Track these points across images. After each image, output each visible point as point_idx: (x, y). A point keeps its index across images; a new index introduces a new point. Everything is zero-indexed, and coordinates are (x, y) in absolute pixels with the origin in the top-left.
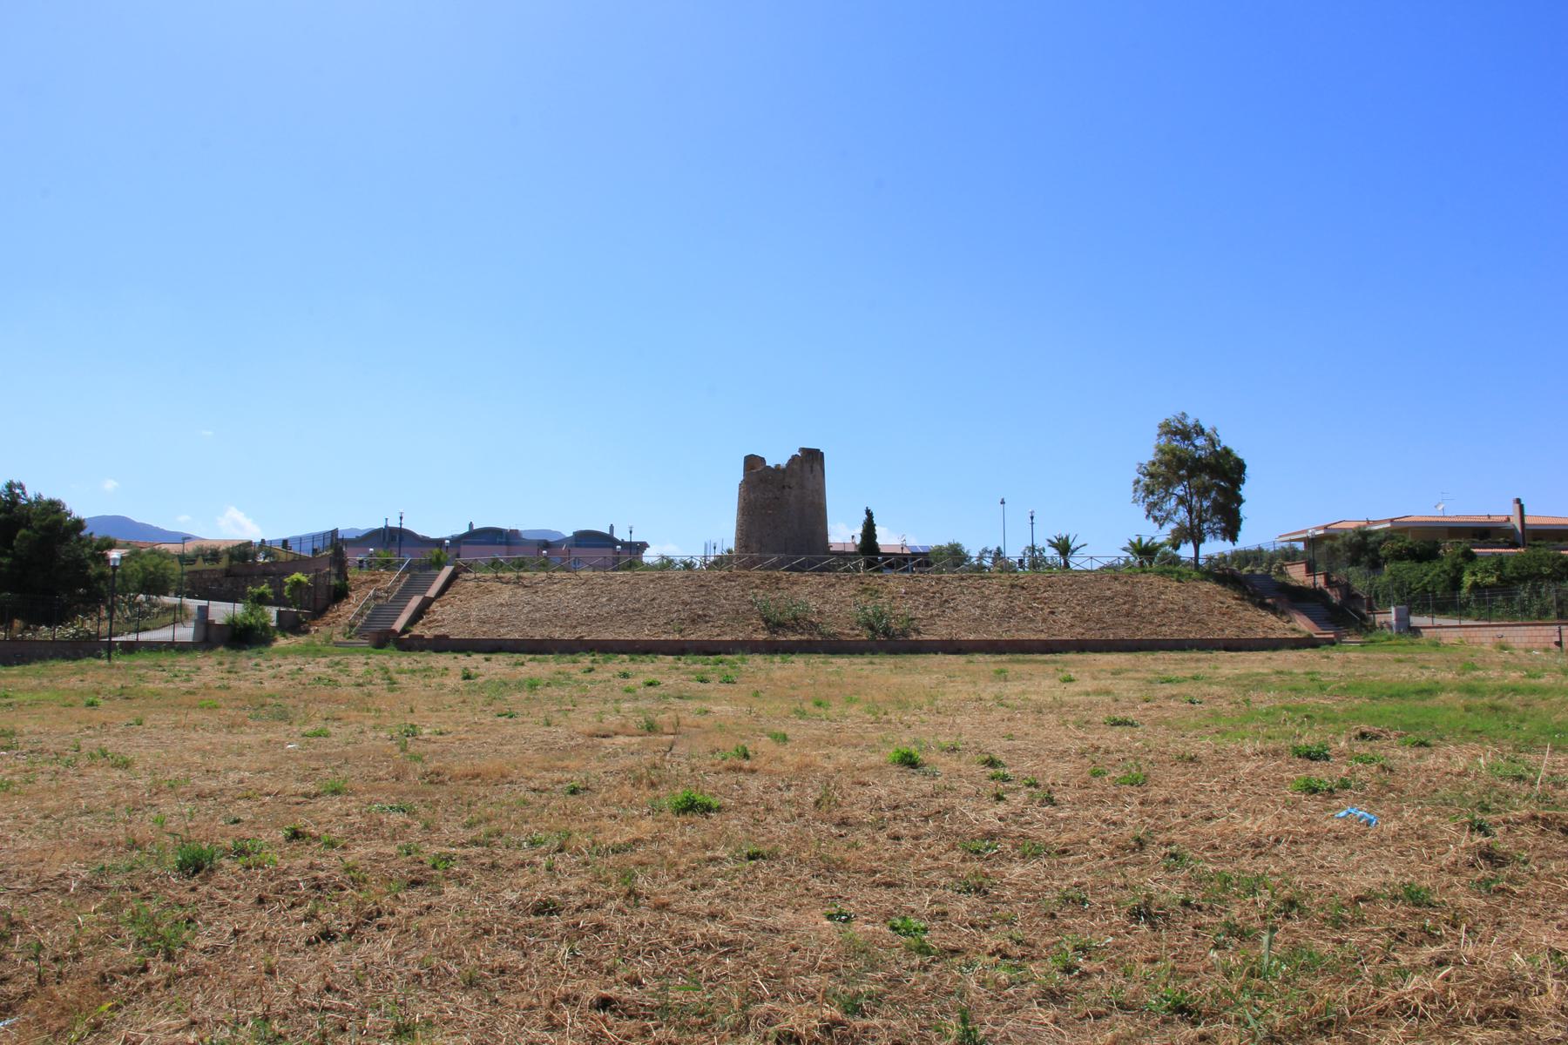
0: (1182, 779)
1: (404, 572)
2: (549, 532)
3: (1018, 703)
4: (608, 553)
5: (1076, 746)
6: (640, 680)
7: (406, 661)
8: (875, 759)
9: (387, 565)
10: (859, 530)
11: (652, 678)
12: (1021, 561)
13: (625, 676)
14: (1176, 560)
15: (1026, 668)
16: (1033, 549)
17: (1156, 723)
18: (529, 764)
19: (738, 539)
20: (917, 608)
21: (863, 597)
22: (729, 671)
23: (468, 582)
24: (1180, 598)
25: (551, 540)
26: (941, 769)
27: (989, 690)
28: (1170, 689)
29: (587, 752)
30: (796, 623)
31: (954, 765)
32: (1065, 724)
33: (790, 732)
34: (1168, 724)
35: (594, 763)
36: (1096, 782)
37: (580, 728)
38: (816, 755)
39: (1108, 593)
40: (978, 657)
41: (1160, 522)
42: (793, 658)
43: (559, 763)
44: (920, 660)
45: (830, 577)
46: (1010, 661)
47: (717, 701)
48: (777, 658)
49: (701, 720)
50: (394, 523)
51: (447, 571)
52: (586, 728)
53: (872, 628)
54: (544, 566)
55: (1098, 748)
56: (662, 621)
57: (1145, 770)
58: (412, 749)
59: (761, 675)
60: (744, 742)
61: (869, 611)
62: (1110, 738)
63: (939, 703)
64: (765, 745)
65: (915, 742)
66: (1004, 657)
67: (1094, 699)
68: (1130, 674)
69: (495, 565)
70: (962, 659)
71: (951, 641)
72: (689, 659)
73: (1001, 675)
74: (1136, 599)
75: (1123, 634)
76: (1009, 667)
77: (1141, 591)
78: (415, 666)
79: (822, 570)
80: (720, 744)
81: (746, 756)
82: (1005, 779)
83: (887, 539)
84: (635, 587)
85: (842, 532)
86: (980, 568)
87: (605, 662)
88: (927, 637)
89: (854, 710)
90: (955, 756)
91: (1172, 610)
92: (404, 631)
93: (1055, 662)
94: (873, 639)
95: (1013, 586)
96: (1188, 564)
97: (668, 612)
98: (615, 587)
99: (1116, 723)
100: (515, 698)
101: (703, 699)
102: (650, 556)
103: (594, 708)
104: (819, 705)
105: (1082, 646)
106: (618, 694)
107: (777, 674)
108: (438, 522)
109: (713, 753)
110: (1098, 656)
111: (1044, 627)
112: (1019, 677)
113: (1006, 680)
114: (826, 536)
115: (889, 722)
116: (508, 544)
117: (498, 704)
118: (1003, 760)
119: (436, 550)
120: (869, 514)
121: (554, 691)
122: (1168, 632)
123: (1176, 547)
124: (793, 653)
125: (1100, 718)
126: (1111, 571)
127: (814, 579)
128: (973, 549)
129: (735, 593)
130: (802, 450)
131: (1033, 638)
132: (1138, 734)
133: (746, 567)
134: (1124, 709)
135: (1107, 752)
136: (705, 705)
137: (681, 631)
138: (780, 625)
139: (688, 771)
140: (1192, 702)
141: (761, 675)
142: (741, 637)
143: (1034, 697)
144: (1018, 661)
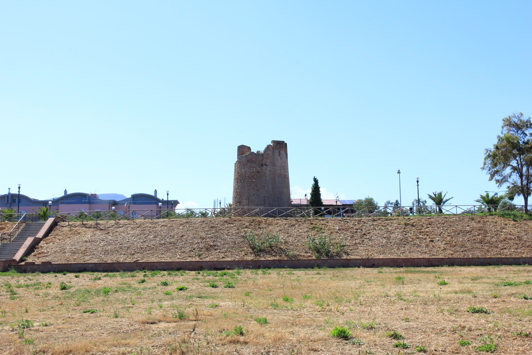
0: (521, 349)
1: (22, 222)
2: (116, 195)
3: (411, 298)
4: (154, 207)
5: (449, 326)
6: (175, 287)
7: (23, 279)
8: (322, 334)
9: (10, 218)
10: (309, 191)
11: (182, 285)
12: (411, 209)
13: (165, 284)
14: (512, 208)
15: (416, 276)
16: (418, 201)
17: (502, 312)
18: (104, 343)
19: (235, 198)
20: (346, 239)
21: (313, 233)
22: (230, 280)
23: (64, 228)
24: (515, 231)
25: (118, 200)
26: (363, 341)
27: (393, 290)
28: (513, 290)
29: (141, 334)
30: (271, 249)
31: (372, 338)
32: (442, 311)
33: (269, 318)
34: (510, 312)
35: (146, 341)
36: (464, 349)
37: (136, 319)
38: (284, 332)
39: (468, 228)
40: (385, 269)
41: (500, 182)
42: (270, 271)
43: (123, 342)
44: (348, 271)
45: (292, 221)
46: (406, 272)
47: (222, 299)
48: (260, 272)
49: (212, 311)
50: (14, 191)
51: (50, 221)
52: (141, 318)
53: (318, 252)
54: (113, 216)
55: (464, 327)
56: (188, 249)
57: (495, 341)
58: (27, 336)
59: (250, 282)
60: (239, 325)
61: (317, 241)
62: (473, 321)
63: (361, 299)
64: (253, 327)
65: (347, 323)
66: (402, 269)
67: (460, 295)
68: (484, 280)
69: (81, 216)
70: (375, 271)
71: (368, 259)
72: (205, 273)
73: (400, 281)
74: (486, 232)
75: (478, 254)
76: (405, 275)
77: (490, 227)
78: (29, 282)
79: (287, 216)
80: (225, 326)
81: (242, 334)
82: (405, 347)
83: (327, 197)
84: (171, 229)
85: (299, 193)
86: (386, 213)
87: (153, 276)
88: (353, 257)
89: (308, 303)
90: (372, 332)
91: (511, 239)
92: (22, 260)
93: (435, 272)
94: (318, 259)
95: (406, 224)
96: (521, 209)
97: (192, 243)
98: (159, 228)
99: (476, 311)
100: (95, 301)
101: (214, 298)
102: (180, 209)
103: (146, 305)
104: (287, 300)
105: (452, 262)
106: (161, 296)
107: (260, 281)
108: (43, 189)
109: (221, 332)
110: (462, 268)
111: (427, 250)
112: (411, 282)
113: (403, 284)
114: (289, 194)
115: (330, 310)
116: (89, 203)
117: (84, 305)
118: (403, 335)
119: (44, 209)
120: (316, 181)
121: (120, 296)
122: (509, 253)
123: (512, 198)
124: (270, 268)
125: (465, 307)
126: (469, 215)
127: (282, 222)
128: (381, 203)
129: (233, 231)
130: (273, 142)
131: (420, 257)
132: (490, 319)
133: (239, 215)
134: (480, 302)
135: (470, 330)
136: (216, 302)
137: (200, 256)
138: (261, 251)
139: (205, 344)
140: (526, 298)
141: (250, 282)
142: (237, 258)
143: (421, 295)
144: (411, 272)
